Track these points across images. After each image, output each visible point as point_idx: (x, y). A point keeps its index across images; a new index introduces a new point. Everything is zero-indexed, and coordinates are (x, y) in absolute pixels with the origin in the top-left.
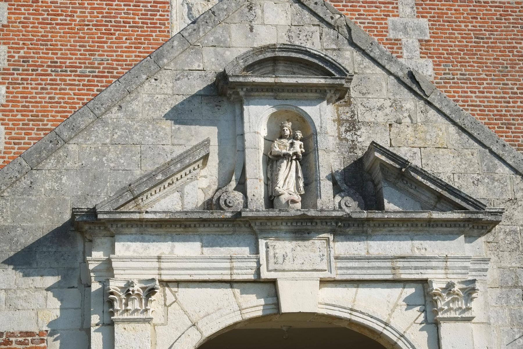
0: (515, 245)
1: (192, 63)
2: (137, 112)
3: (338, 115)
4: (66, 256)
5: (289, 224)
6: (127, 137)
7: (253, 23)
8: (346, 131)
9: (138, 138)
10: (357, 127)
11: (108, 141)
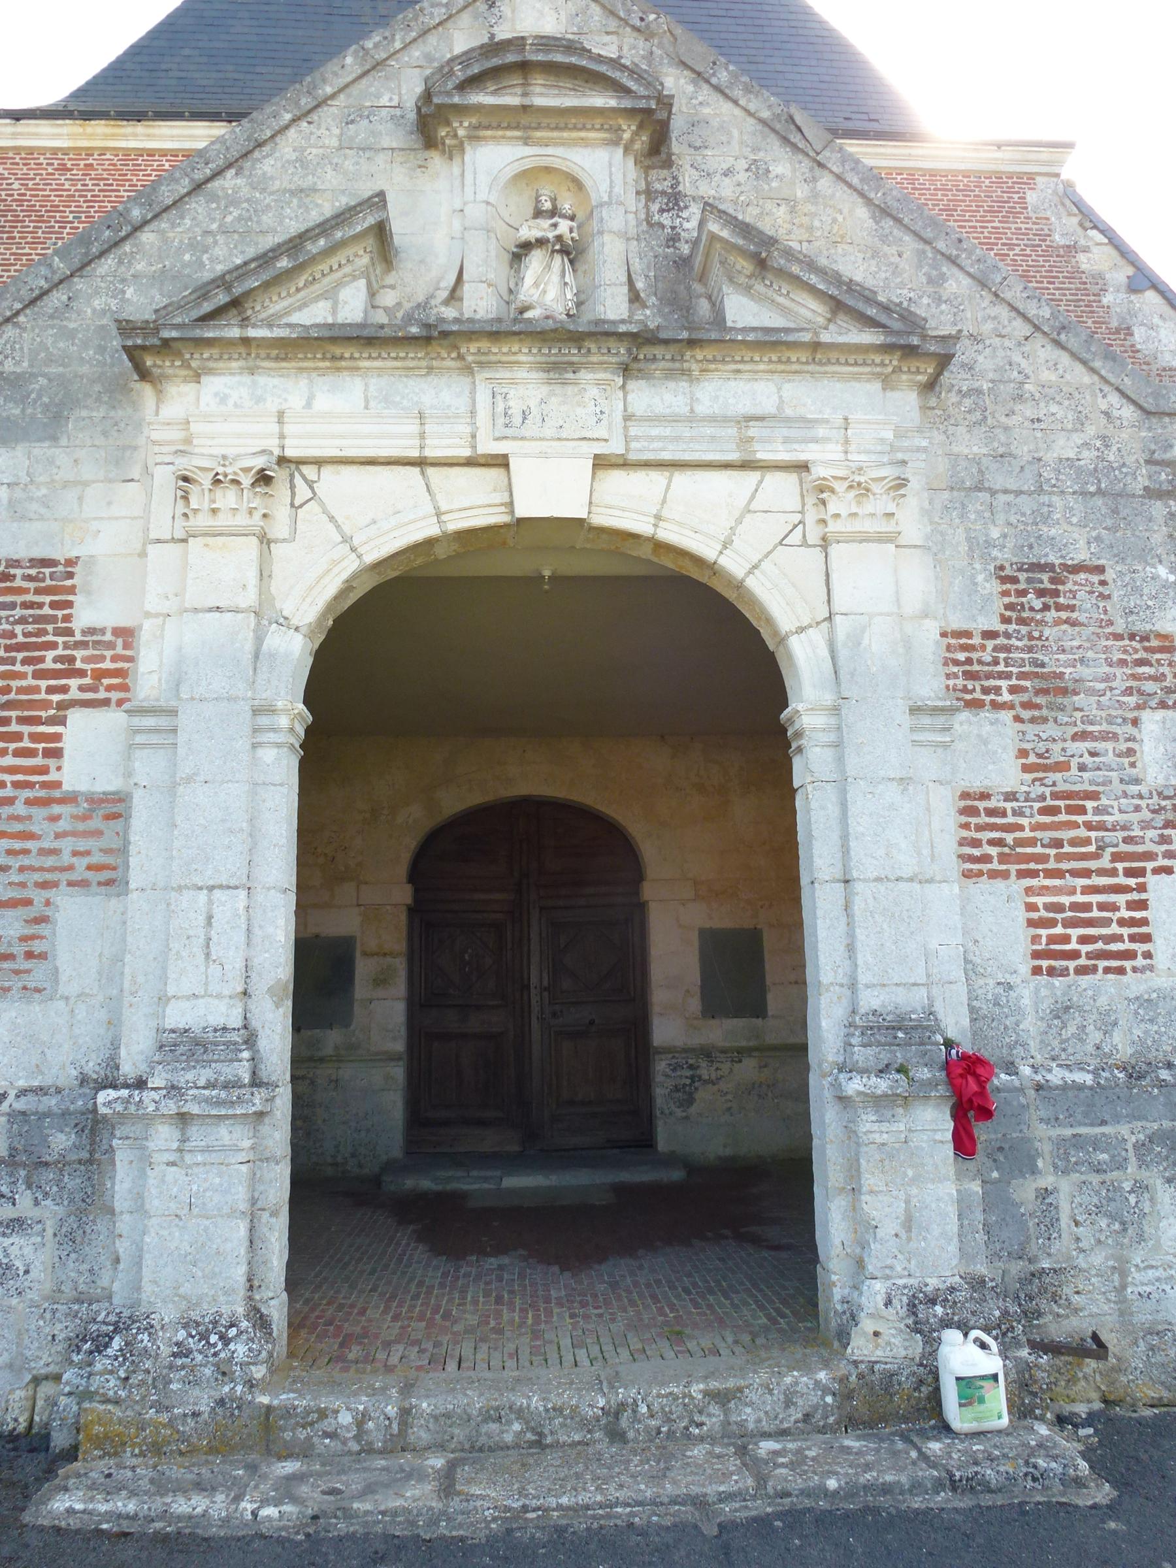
0: (978, 415)
1: (378, 97)
2: (272, 178)
3: (648, 184)
4: (122, 425)
5: (535, 351)
6: (250, 219)
7: (495, 28)
8: (662, 211)
9: (269, 221)
10: (682, 204)
11: (214, 226)
